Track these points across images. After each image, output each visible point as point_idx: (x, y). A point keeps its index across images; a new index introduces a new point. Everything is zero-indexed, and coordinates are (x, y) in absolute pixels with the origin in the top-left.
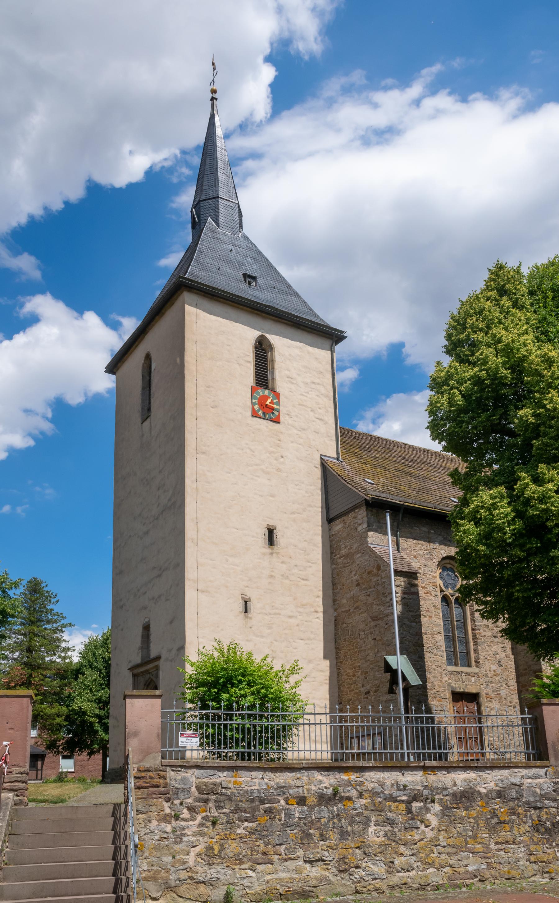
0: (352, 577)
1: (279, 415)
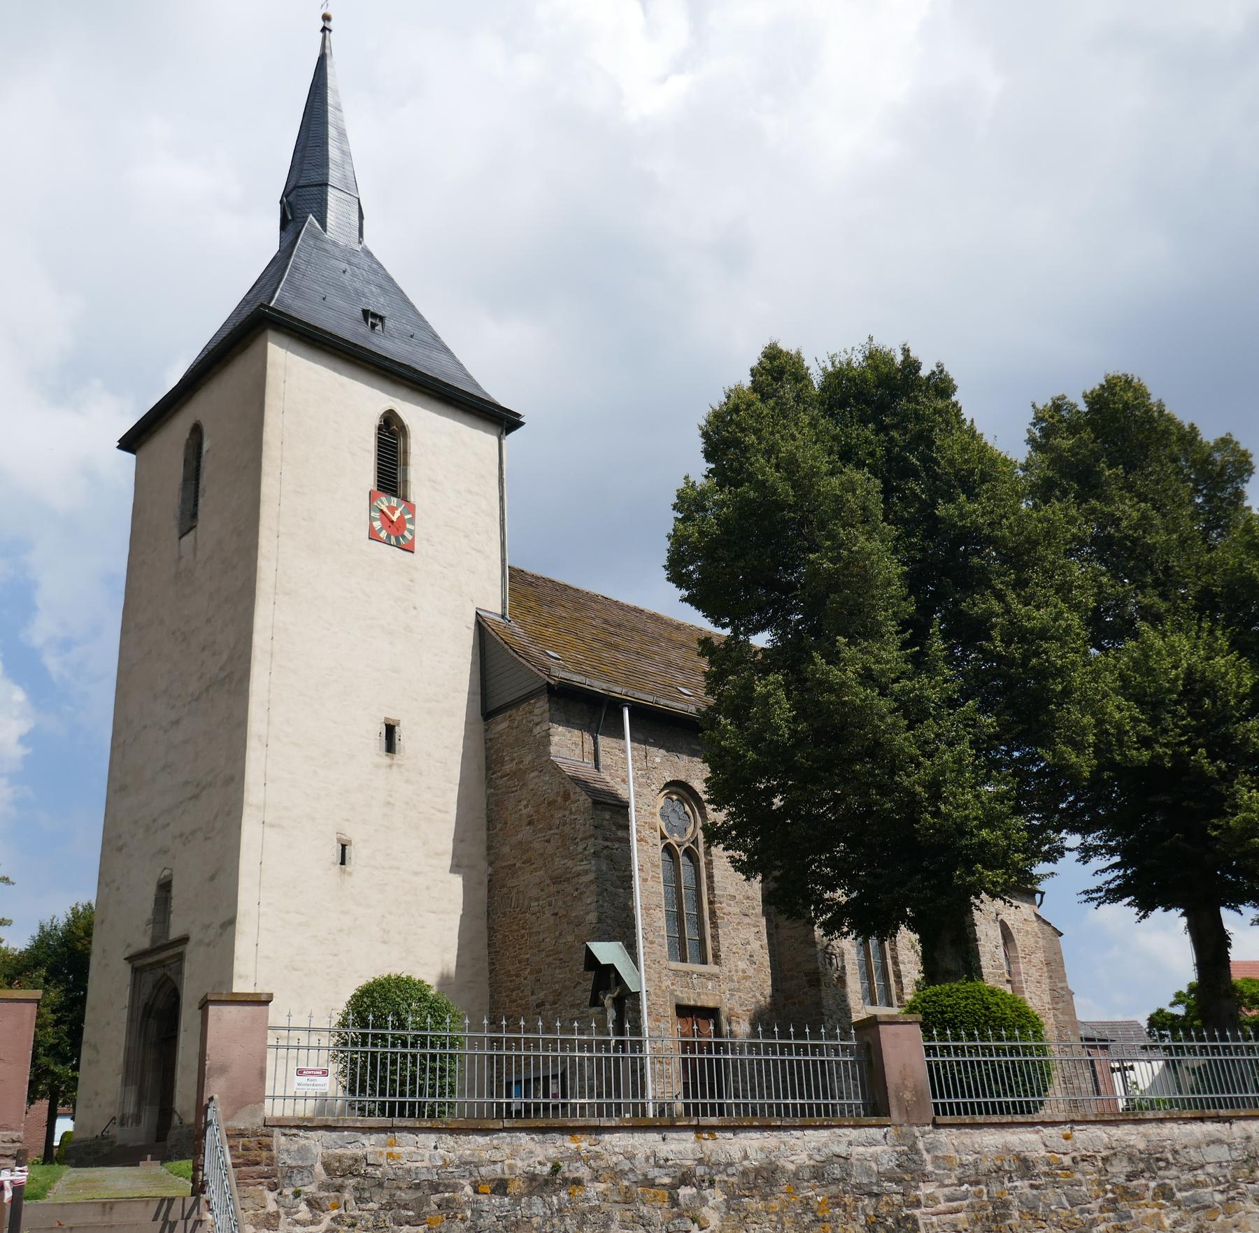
1: (413, 539)
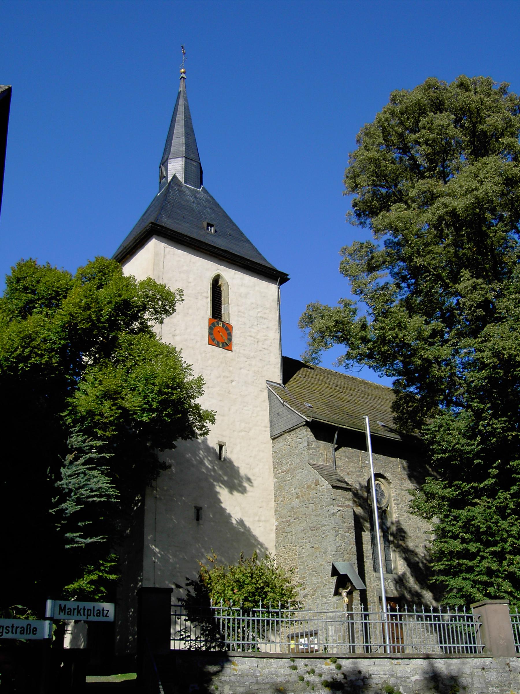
0: (292, 490)
